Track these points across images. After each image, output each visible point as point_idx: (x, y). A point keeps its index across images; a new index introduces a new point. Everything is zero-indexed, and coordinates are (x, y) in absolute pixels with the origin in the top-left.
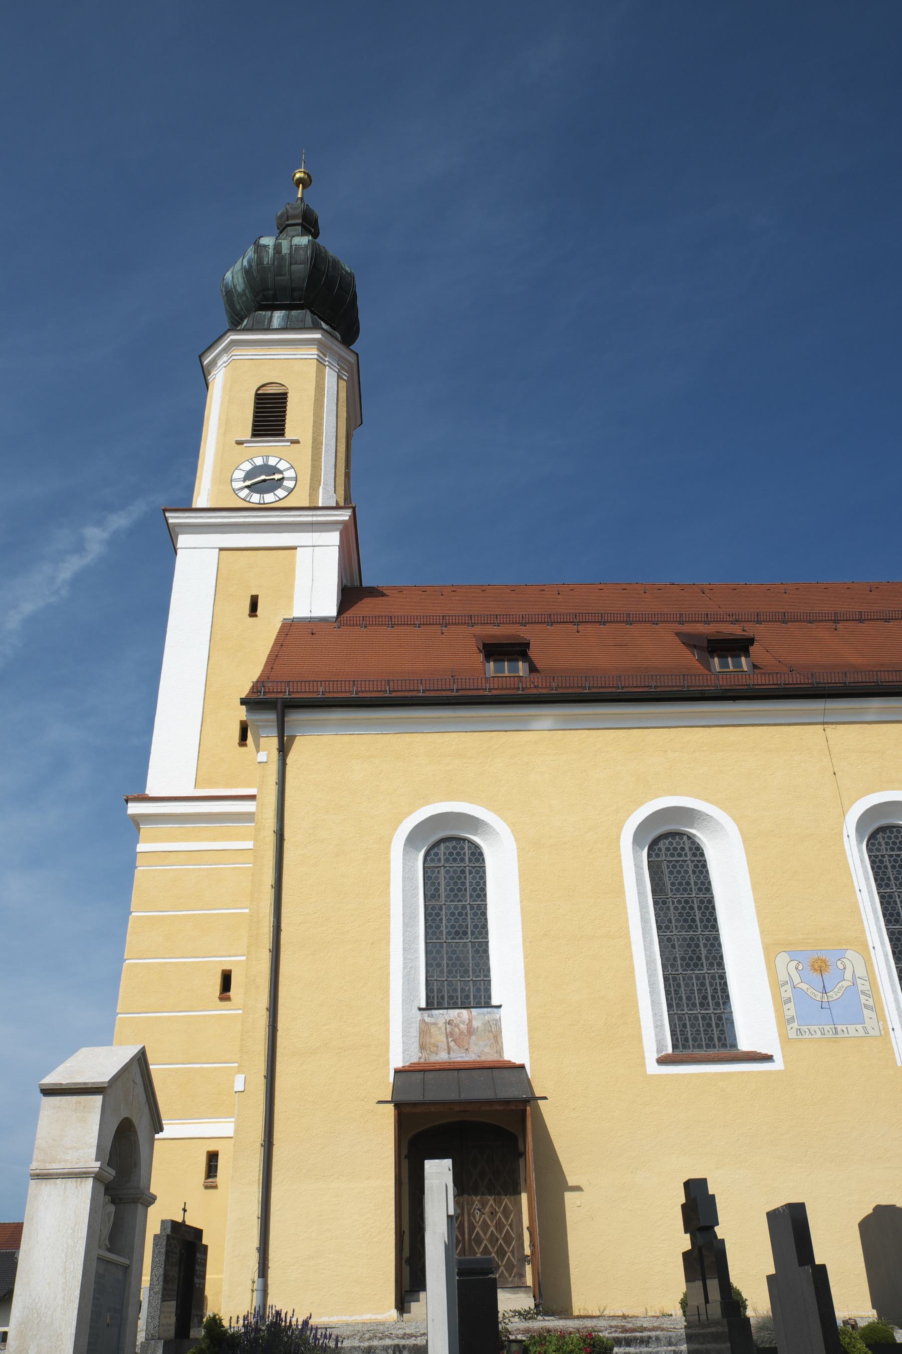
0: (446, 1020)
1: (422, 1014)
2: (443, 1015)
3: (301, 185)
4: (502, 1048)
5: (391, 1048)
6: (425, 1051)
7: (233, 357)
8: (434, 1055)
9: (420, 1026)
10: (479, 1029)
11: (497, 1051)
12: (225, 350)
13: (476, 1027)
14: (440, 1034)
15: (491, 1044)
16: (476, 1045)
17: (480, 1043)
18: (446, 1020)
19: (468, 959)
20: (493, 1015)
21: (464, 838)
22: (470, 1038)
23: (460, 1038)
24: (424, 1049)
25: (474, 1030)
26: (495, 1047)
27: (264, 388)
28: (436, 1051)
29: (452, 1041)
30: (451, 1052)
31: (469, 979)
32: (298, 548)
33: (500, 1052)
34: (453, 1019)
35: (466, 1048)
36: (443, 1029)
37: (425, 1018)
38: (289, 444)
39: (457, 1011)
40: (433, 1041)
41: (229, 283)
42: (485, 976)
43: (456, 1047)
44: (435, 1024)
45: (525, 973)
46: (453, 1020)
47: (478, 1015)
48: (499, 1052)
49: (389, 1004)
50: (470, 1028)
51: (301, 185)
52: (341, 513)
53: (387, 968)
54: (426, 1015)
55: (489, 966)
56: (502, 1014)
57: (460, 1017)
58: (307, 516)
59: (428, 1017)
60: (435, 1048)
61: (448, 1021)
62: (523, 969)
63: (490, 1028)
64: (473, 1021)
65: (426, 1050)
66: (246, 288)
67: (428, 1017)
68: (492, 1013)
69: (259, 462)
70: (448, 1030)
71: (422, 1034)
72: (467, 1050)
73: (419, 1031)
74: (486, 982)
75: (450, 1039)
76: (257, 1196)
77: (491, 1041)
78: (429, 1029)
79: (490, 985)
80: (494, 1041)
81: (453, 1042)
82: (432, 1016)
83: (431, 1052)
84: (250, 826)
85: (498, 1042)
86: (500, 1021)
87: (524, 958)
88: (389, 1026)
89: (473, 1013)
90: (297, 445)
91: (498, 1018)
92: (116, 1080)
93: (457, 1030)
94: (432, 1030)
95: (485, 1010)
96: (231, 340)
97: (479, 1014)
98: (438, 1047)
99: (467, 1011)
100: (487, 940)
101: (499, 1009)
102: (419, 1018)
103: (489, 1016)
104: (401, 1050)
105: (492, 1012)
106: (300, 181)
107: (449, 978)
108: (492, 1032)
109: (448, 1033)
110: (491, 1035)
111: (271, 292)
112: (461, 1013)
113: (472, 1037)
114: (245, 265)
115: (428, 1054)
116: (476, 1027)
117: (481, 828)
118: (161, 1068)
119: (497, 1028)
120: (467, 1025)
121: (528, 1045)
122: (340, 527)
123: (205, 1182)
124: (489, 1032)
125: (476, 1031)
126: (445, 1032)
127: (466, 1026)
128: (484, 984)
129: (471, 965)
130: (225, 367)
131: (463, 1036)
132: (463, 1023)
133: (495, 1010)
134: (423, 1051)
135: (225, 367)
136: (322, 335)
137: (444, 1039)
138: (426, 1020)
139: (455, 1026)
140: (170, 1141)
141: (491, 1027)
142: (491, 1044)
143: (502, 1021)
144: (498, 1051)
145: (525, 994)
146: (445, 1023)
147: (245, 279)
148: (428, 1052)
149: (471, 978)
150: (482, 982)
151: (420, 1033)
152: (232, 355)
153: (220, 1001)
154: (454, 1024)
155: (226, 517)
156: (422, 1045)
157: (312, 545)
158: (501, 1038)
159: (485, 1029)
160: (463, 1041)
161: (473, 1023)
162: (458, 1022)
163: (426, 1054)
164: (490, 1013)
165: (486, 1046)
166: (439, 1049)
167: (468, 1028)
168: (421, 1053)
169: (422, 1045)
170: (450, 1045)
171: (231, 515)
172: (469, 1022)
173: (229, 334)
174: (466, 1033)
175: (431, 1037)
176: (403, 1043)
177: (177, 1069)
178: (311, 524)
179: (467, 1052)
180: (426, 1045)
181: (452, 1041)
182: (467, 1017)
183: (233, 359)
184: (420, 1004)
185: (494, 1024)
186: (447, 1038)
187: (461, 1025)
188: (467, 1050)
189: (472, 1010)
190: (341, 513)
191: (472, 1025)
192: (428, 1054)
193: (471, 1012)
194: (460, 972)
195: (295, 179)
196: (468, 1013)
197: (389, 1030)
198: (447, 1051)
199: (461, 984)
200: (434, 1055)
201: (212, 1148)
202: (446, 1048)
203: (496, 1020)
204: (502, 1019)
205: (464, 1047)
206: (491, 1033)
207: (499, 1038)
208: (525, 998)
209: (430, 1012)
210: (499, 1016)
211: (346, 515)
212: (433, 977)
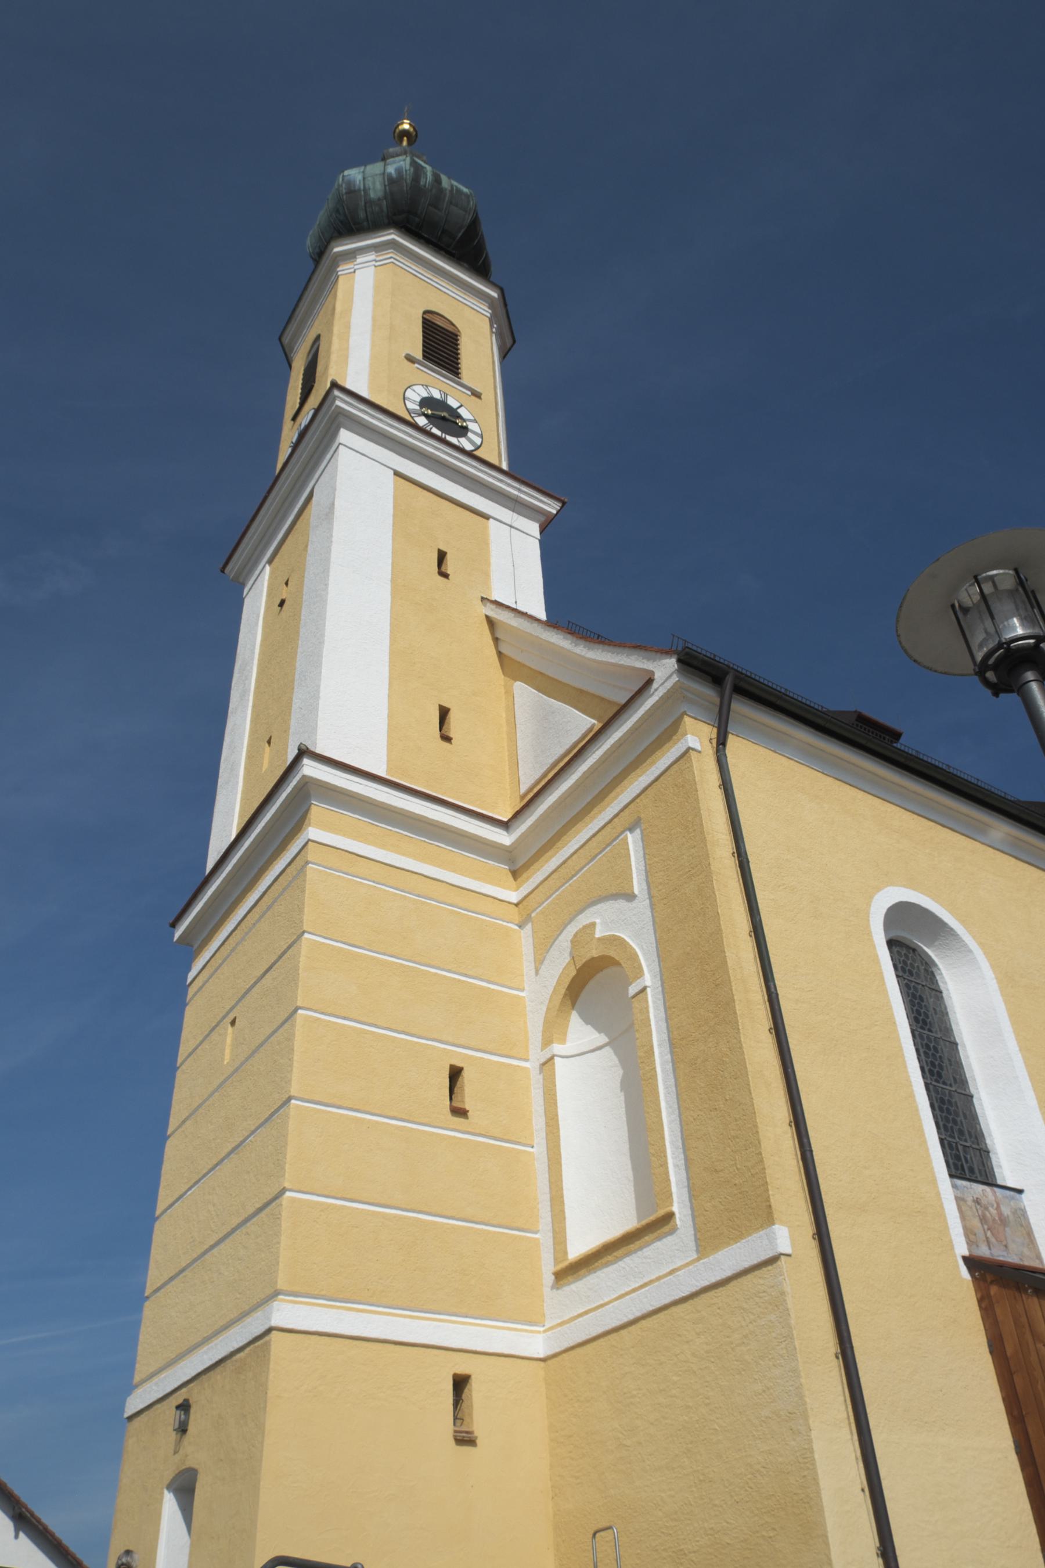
3: (405, 138)
7: (392, 260)
12: (377, 248)
21: (912, 946)
27: (431, 315)
32: (491, 520)
38: (469, 393)
41: (402, 172)
51: (405, 138)
52: (549, 502)
58: (509, 485)
61: (975, 1199)
66: (385, 197)
69: (437, 395)
76: (852, 1448)
84: (469, 857)
90: (477, 399)
92: (958, 1157)
96: (393, 239)
106: (405, 133)
111: (417, 220)
114: (391, 174)
117: (943, 938)
118: (369, 1211)
122: (543, 519)
123: (455, 1432)
130: (375, 266)
135: (375, 266)
136: (498, 295)
140: (393, 1346)
147: (387, 188)
152: (391, 258)
153: (452, 1115)
155: (410, 436)
157: (509, 523)
171: (418, 436)
173: (392, 231)
177: (395, 1216)
178: (513, 499)
183: (393, 262)
190: (549, 502)
195: (397, 131)
201: (462, 1370)
211: (554, 508)
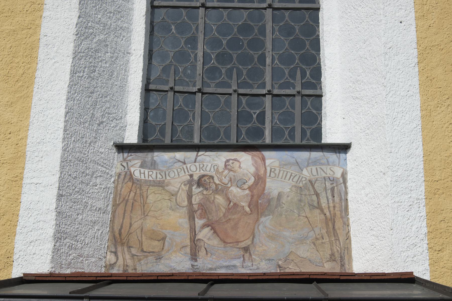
0: (191, 176)
1: (124, 160)
2: (184, 163)
4: (348, 249)
5: (22, 222)
6: (126, 249)
8: (151, 258)
9: (116, 188)
10: (284, 200)
11: (332, 255)
13: (275, 193)
14: (171, 208)
15: (317, 239)
16: (272, 238)
17: (286, 233)
18: (191, 176)
19: (262, 45)
20: (324, 167)
22: (258, 220)
23: (228, 221)
24: (123, 244)
25: (269, 201)
26: (327, 246)
28: (156, 250)
29: (204, 226)
30: (202, 253)
31: (264, 91)
33: (342, 258)
34: (213, 173)
35: (243, 245)
36: (183, 197)
37: (132, 169)
39: (224, 156)
40: (149, 223)
42: (305, 85)
43: (215, 242)
44: (161, 185)
45: (420, 54)
46: (212, 177)
47: (282, 165)
48: (338, 259)
49: (28, 116)
50: (259, 197)
53: (31, 31)
54: (138, 162)
55: (319, 64)
56: (350, 166)
57: (230, 170)
59: (142, 166)
60: (156, 243)
61: (196, 178)
62: (415, 45)
63: (314, 198)
64: (268, 180)
65: (129, 247)
67: (142, 166)
68: (323, 164)
70: (196, 200)
71: (122, 205)
72: (246, 249)
73: (115, 200)
74: (309, 101)
75: (199, 222)
77: (317, 230)
78: (141, 195)
79: (319, 108)
80: (324, 231)
81: (207, 230)
82: (153, 165)
83: (142, 251)
85: (336, 234)
86: (345, 182)
87: (417, 19)
88: (24, 168)
89: (268, 162)
91: (338, 174)
93: (220, 199)
94: (151, 198)
95: (303, 155)
97: (283, 165)
98: (164, 239)
99: (253, 156)
100: (317, 92)
101: (342, 155)
102: (117, 168)
103: (314, 168)
104: (50, 231)
105: (324, 161)
107: (209, 86)
108: (319, 207)
109: (196, 207)
110: (317, 216)
112: (235, 160)
113: (263, 219)
115: (133, 256)
116: (275, 193)
119: (337, 199)
120: (250, 188)
121: (425, 230)
124: (312, 207)
125: (274, 203)
126: (186, 203)
127: (247, 192)
128: (304, 104)
129: (268, 61)
131: (235, 216)
132: (240, 183)
133: (332, 156)
134: (119, 249)
137: (184, 222)
138: (137, 174)
139: (217, 191)
141: (317, 195)
142: (317, 239)
143: (349, 184)
144: (337, 255)
145: (418, 103)
146: (190, 183)
148: (134, 251)
149: (268, 87)
150: (298, 99)
151: (115, 205)
154: (214, 186)
156: (120, 234)
158: (347, 224)
159: (300, 201)
160: (235, 227)
161: (268, 185)
162: (226, 181)
163: (128, 256)
164: (316, 162)
165: (302, 241)
166: (166, 243)
167: (252, 196)
168: (115, 253)
169: (120, 234)
170: (200, 236)
172: (256, 183)
174: (247, 209)
175: (145, 215)
176: (59, 213)
179: (247, 255)
180: (129, 234)
181: (204, 226)
182: (252, 170)
184: (123, 138)
185: (325, 189)
186: (192, 218)
187: (234, 190)
188: (246, 249)
189: (267, 154)
191: (264, 189)
192: (133, 256)
193: (264, 159)
194: (239, 75)
196: (256, 162)
197: (22, 179)
198: (188, 250)
199: (239, 103)
200: (151, 258)
202: (188, 242)
203: (333, 180)
204: (349, 176)
205: (238, 242)
206: (318, 211)
207: (339, 224)
208: (418, 113)
209: (149, 156)
210: (341, 170)
212: (167, 82)
